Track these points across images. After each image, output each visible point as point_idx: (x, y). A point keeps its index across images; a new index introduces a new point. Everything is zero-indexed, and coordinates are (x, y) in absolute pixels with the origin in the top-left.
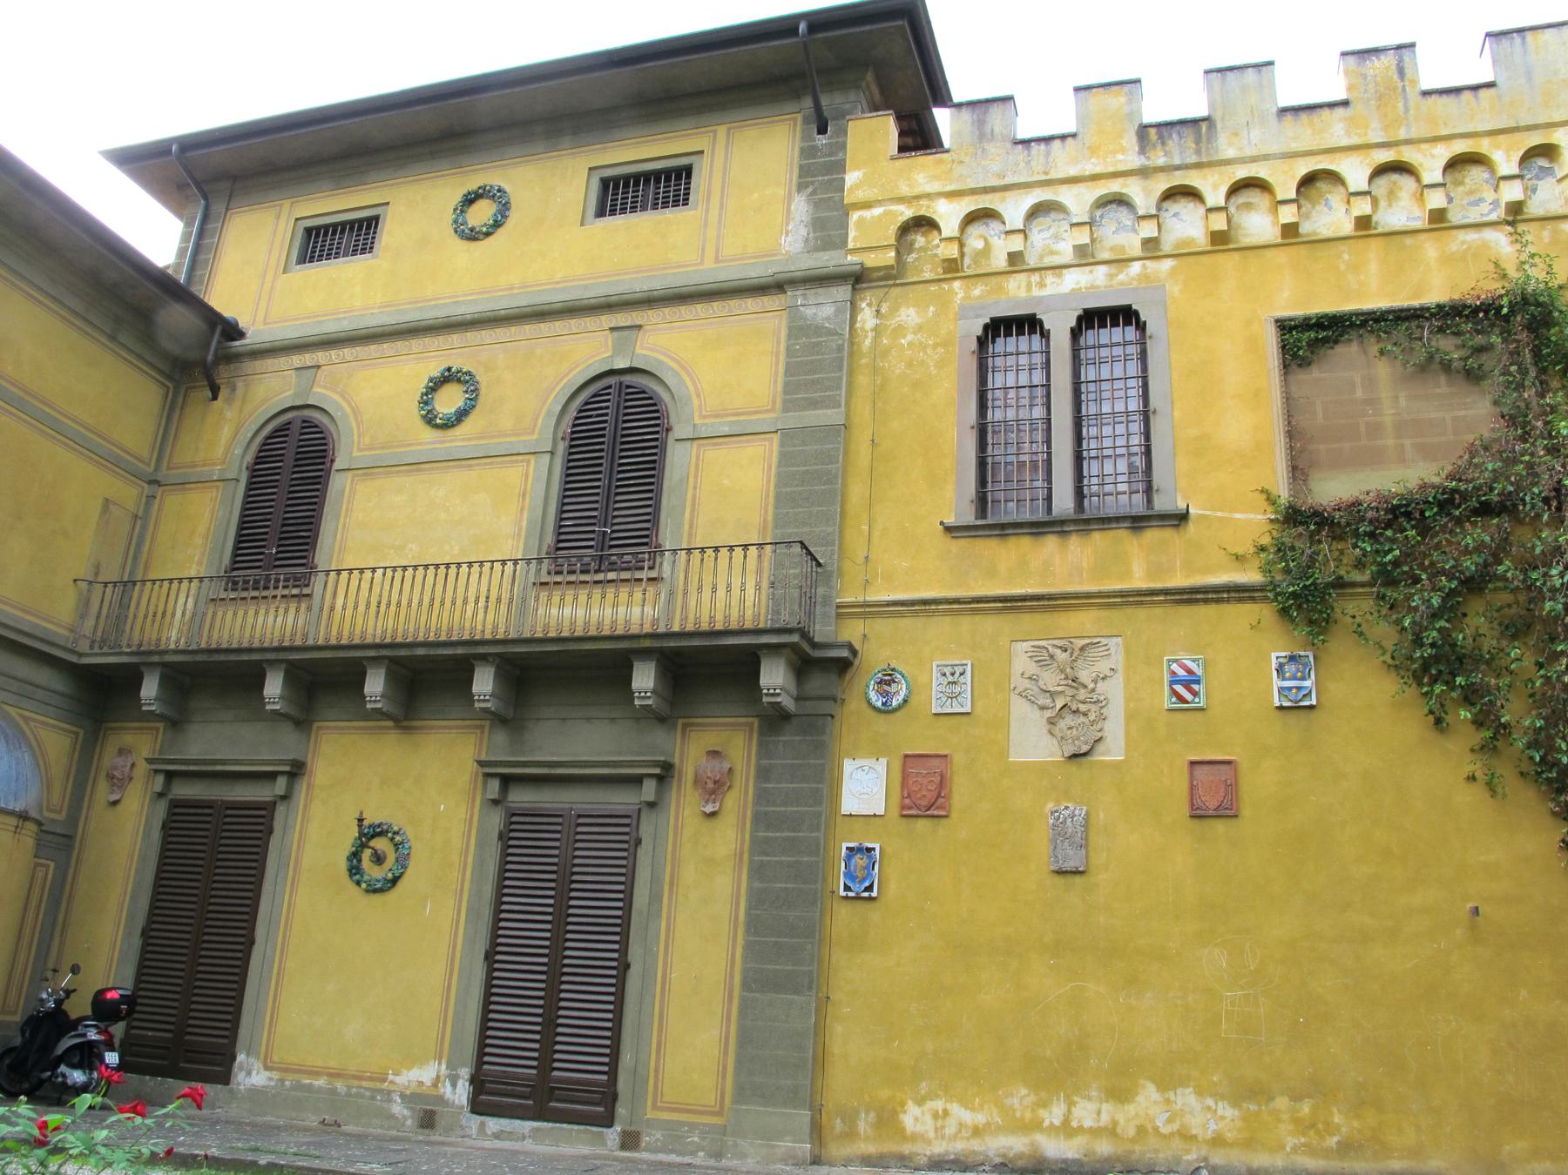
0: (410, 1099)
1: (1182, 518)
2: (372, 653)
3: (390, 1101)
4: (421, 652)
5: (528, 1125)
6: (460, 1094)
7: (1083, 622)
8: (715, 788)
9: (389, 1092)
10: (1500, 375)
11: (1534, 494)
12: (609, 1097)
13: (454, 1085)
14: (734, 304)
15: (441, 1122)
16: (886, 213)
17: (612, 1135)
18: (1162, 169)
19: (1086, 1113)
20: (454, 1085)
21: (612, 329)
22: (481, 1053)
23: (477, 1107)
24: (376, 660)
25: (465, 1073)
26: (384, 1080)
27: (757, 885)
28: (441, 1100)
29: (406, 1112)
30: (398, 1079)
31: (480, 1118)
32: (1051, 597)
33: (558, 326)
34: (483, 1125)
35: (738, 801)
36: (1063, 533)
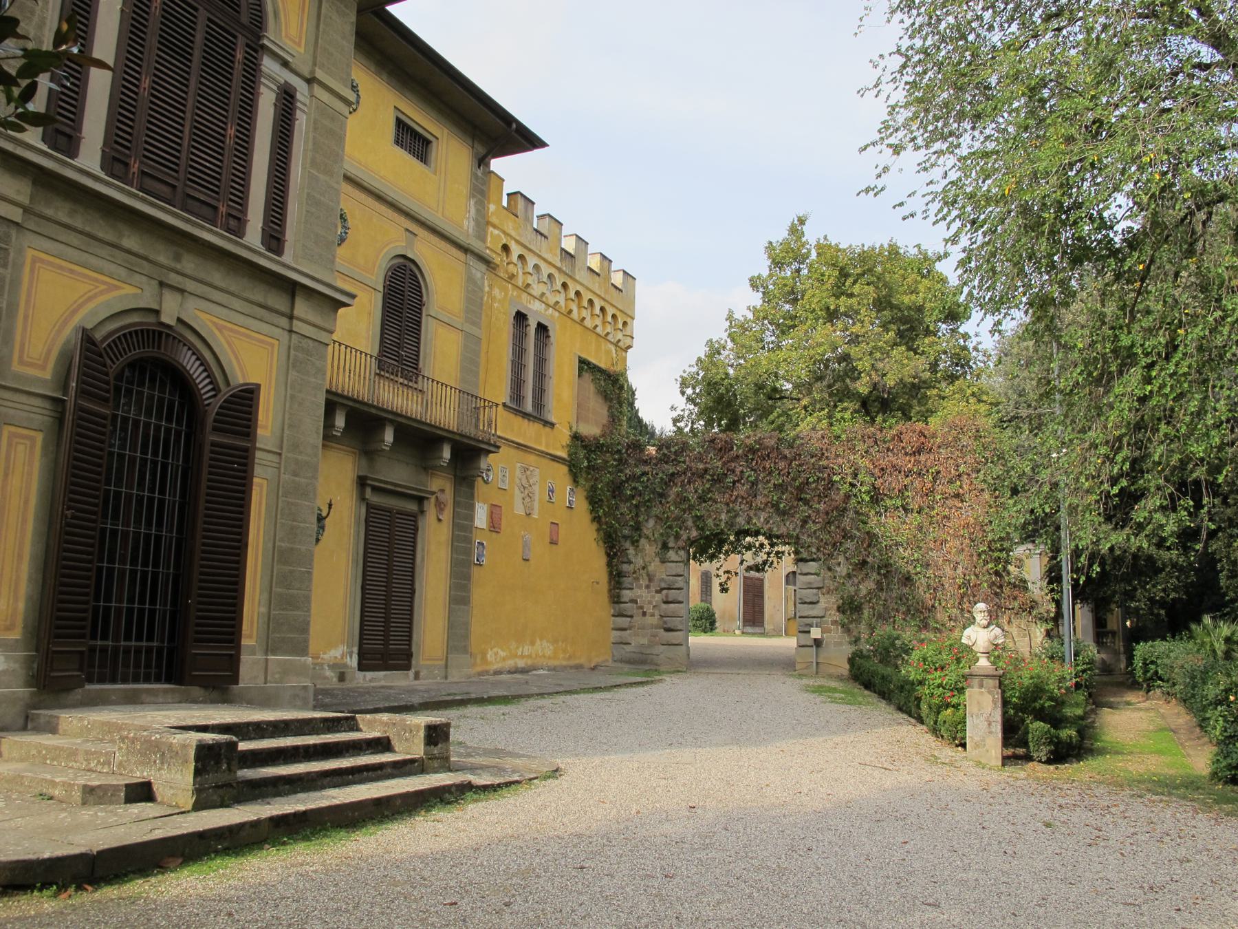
0: (333, 667)
1: (552, 425)
2: (390, 417)
3: (323, 669)
4: (373, 411)
5: (382, 673)
6: (353, 662)
7: (532, 459)
8: (440, 506)
9: (323, 664)
10: (1209, 719)
11: (1228, 698)
12: (408, 655)
13: (351, 657)
14: (448, 247)
15: (348, 677)
16: (499, 235)
17: (411, 673)
18: (567, 274)
19: (527, 650)
20: (351, 657)
21: (407, 230)
22: (361, 639)
23: (361, 667)
24: (392, 421)
25: (356, 650)
26: (318, 658)
27: (455, 556)
28: (345, 665)
29: (332, 674)
30: (326, 657)
31: (364, 673)
32: (525, 446)
33: (383, 209)
34: (365, 676)
35: (447, 515)
36: (529, 420)
